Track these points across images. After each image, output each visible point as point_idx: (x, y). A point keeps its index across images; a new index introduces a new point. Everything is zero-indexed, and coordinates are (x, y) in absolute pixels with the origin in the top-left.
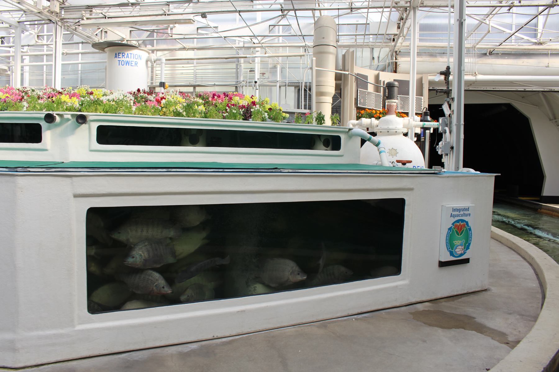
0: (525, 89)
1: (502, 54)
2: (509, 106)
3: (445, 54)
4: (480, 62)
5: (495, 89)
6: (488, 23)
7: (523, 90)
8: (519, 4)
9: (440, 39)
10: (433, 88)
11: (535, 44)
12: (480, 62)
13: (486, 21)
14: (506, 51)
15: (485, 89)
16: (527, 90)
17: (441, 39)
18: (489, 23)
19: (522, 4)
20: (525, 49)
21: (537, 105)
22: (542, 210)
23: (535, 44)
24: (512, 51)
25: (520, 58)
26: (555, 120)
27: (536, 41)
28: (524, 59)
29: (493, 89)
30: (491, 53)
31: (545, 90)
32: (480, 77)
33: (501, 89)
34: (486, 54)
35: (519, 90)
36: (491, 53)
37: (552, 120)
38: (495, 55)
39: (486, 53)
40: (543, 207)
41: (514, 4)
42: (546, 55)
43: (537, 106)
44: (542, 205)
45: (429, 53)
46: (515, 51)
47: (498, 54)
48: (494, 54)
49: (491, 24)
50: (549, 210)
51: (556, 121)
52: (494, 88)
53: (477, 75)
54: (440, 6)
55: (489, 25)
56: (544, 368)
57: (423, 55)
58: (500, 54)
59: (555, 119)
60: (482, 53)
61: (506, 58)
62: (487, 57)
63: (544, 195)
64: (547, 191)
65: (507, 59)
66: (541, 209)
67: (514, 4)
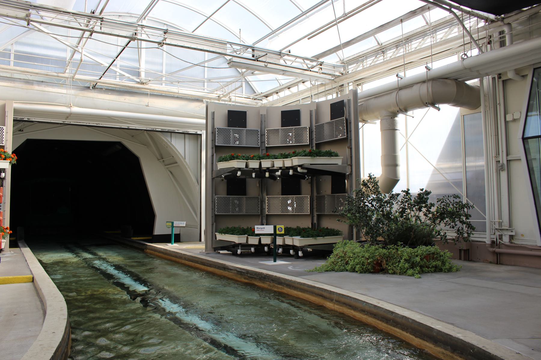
0: (128, 127)
1: (106, 89)
2: (120, 143)
3: (43, 83)
4: (81, 95)
5: (98, 125)
6: (80, 51)
7: (127, 127)
8: (100, 31)
9: (34, 64)
10: (28, 119)
11: (138, 83)
12: (81, 95)
13: (79, 49)
14: (110, 87)
15: (88, 124)
16: (130, 128)
17: (35, 64)
18: (82, 51)
19: (102, 31)
20: (125, 86)
21: (146, 144)
22: (147, 250)
23: (138, 83)
24: (116, 87)
25: (123, 96)
26: (163, 160)
27: (139, 80)
28: (127, 96)
29: (96, 125)
30: (94, 87)
31: (148, 129)
32: (76, 110)
33: (104, 126)
34: (89, 88)
35: (123, 127)
36: (95, 87)
37: (160, 160)
38: (99, 89)
39: (89, 86)
40: (148, 247)
41: (94, 29)
42: (146, 94)
43: (145, 145)
44: (147, 245)
45: (24, 79)
46: (119, 88)
47: (102, 89)
48: (97, 88)
49: (84, 53)
50: (152, 250)
51: (163, 161)
52: (97, 124)
53: (71, 107)
54: (8, 16)
55: (81, 53)
56: (291, 280)
57: (17, 81)
58: (104, 89)
59: (162, 159)
60: (86, 86)
61: (110, 93)
62: (90, 91)
63: (155, 234)
64: (159, 229)
65: (110, 94)
66: (146, 249)
67: (94, 29)
